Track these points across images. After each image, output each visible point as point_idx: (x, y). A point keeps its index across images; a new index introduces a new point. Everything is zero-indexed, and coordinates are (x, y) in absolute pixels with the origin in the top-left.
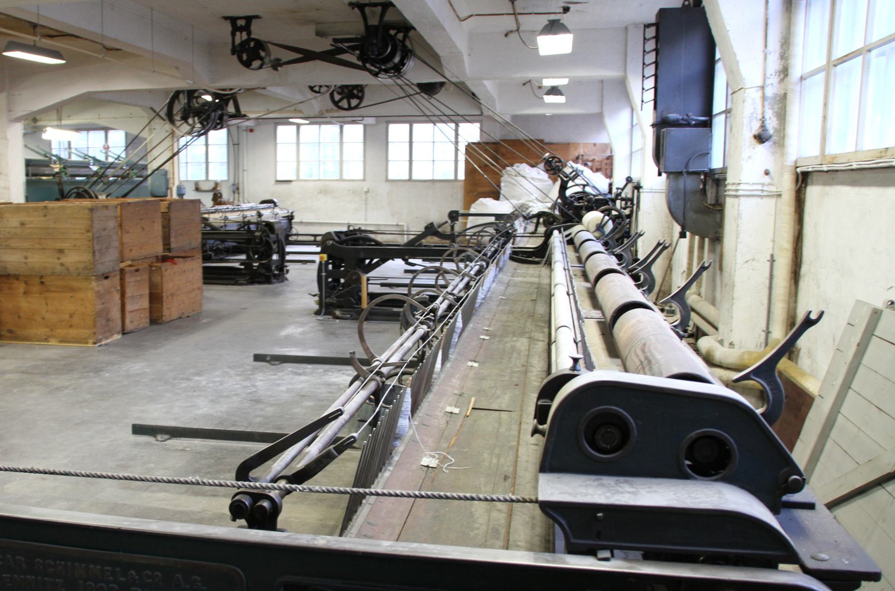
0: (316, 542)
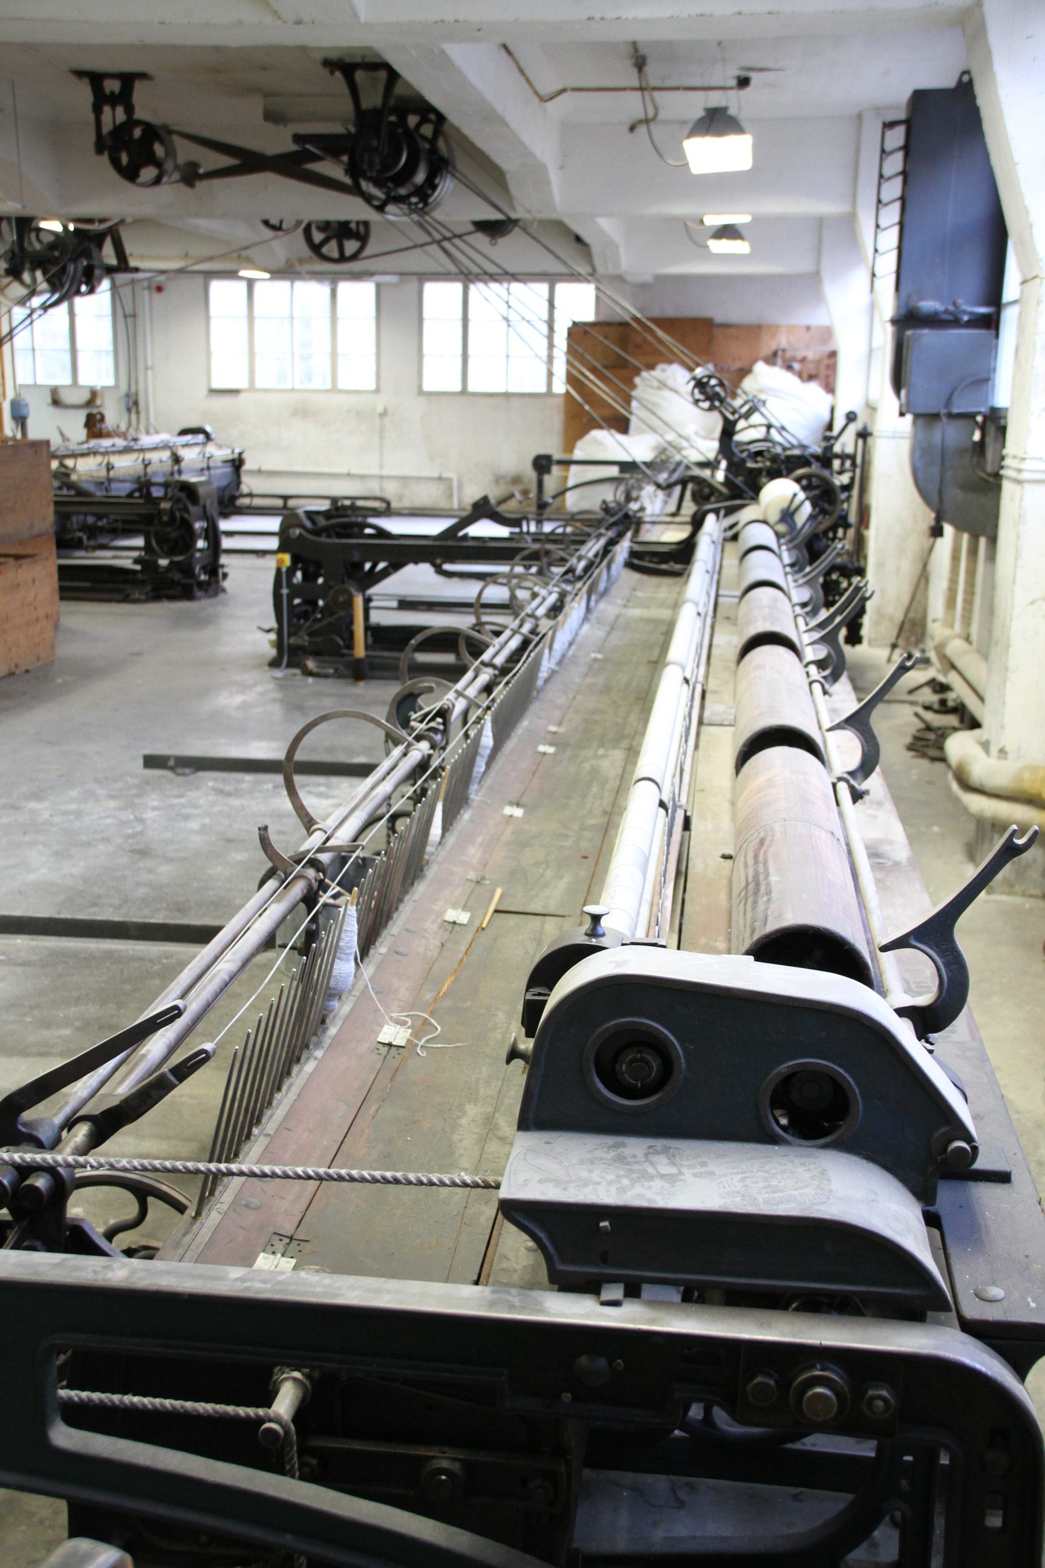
0: (110, 1275)
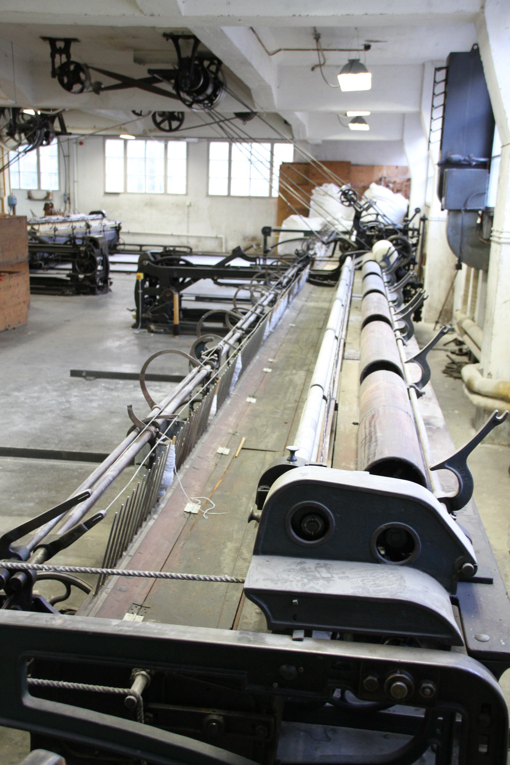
0: (54, 622)
